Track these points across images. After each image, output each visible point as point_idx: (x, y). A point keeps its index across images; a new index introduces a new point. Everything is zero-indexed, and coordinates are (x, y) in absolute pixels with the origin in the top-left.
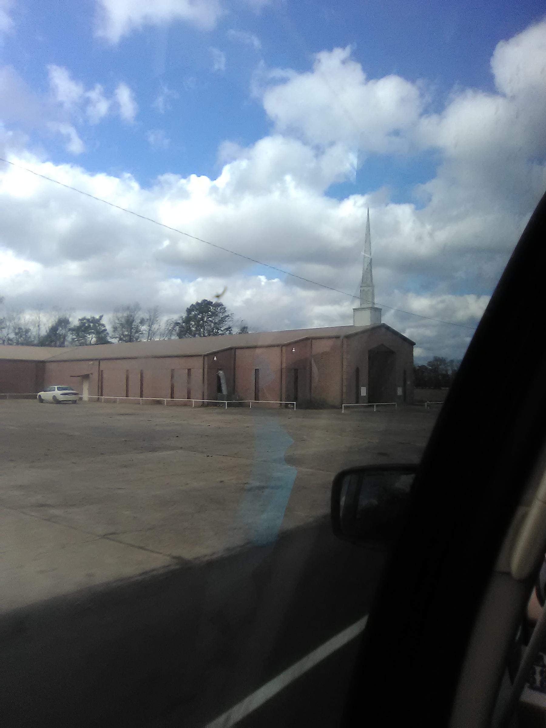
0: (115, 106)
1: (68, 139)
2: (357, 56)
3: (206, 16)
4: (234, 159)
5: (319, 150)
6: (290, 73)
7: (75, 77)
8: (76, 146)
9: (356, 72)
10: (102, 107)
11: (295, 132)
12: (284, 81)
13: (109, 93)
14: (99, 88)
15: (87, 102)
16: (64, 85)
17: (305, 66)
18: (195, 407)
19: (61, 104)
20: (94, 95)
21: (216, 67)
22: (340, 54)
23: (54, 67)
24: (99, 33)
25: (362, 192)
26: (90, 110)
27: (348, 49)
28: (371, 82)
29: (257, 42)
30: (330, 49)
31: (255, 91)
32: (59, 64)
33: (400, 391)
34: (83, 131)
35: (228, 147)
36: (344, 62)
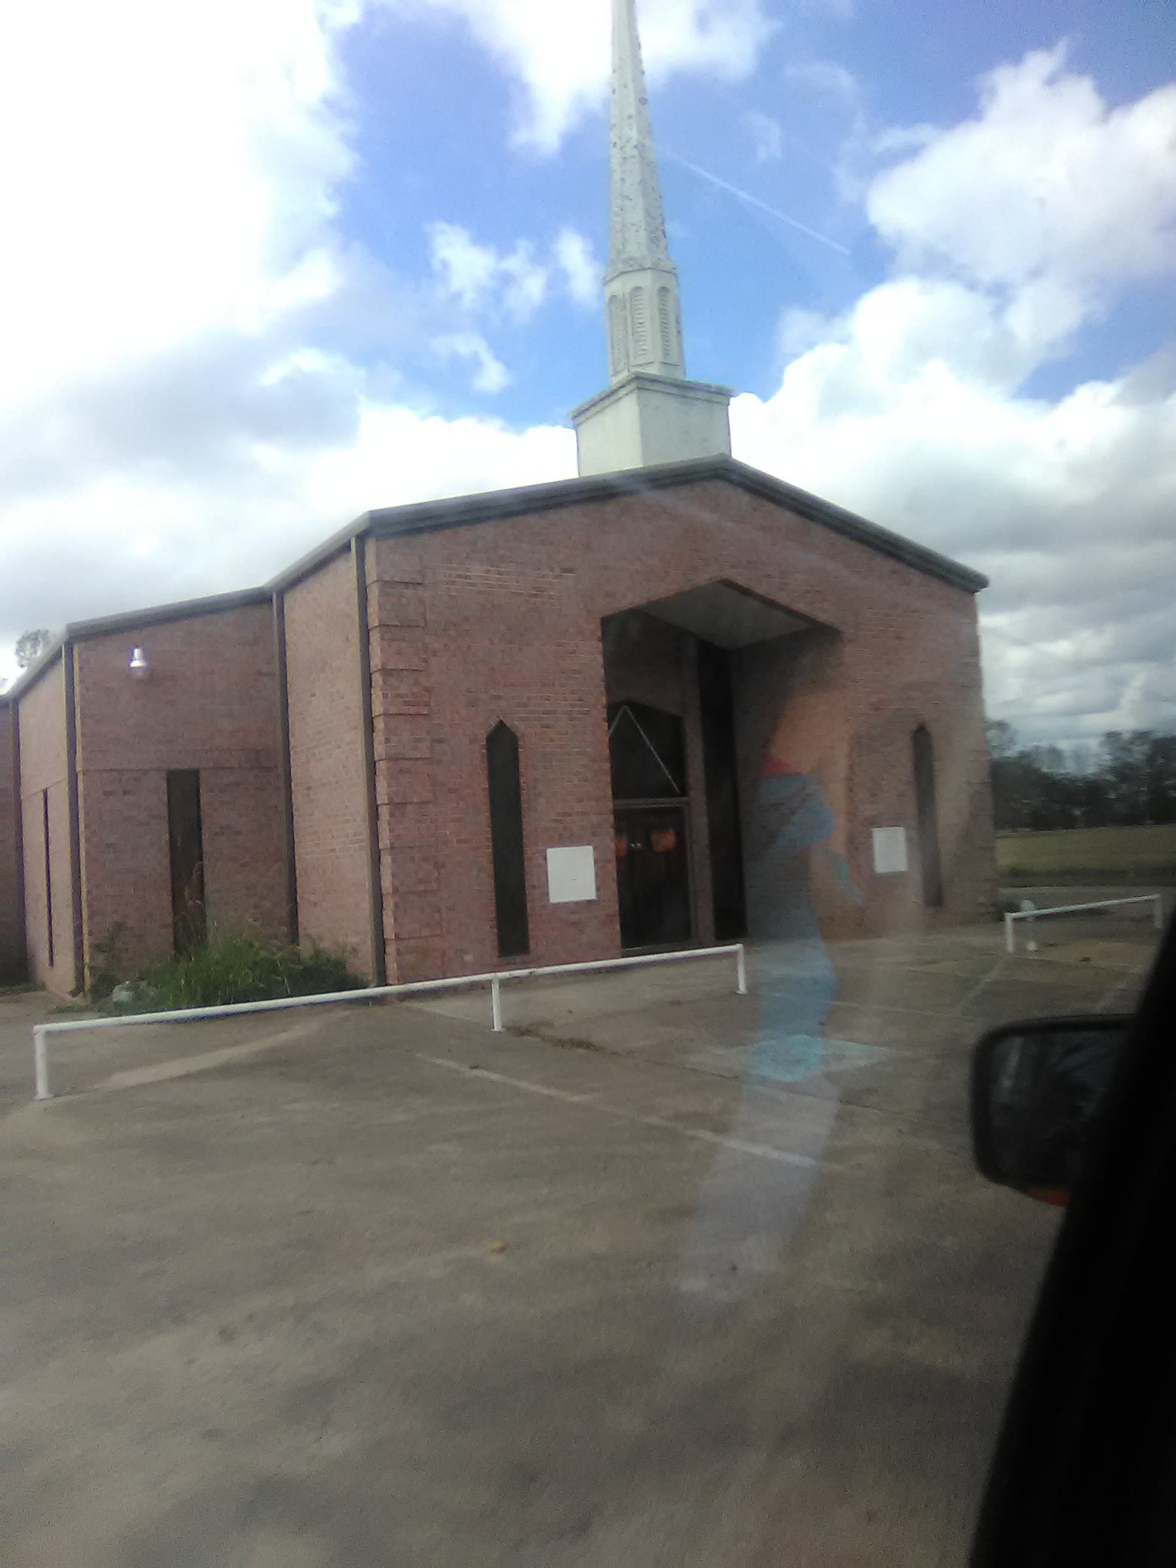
0: (559, 279)
1: (476, 364)
2: (1079, 63)
3: (733, 48)
4: (811, 346)
5: (1000, 294)
6: (924, 132)
7: (480, 238)
8: (493, 376)
9: (1082, 94)
10: (534, 286)
11: (937, 264)
12: (912, 152)
13: (543, 255)
14: (524, 246)
15: (506, 280)
16: (463, 260)
17: (959, 104)
18: (96, 991)
19: (458, 296)
20: (514, 264)
21: (762, 154)
22: (1040, 64)
23: (441, 226)
24: (521, 137)
25: (1103, 371)
26: (513, 299)
27: (1062, 48)
28: (1117, 117)
29: (845, 80)
30: (1016, 58)
31: (845, 183)
32: (450, 221)
33: (891, 850)
34: (503, 344)
35: (796, 323)
36: (1051, 81)
